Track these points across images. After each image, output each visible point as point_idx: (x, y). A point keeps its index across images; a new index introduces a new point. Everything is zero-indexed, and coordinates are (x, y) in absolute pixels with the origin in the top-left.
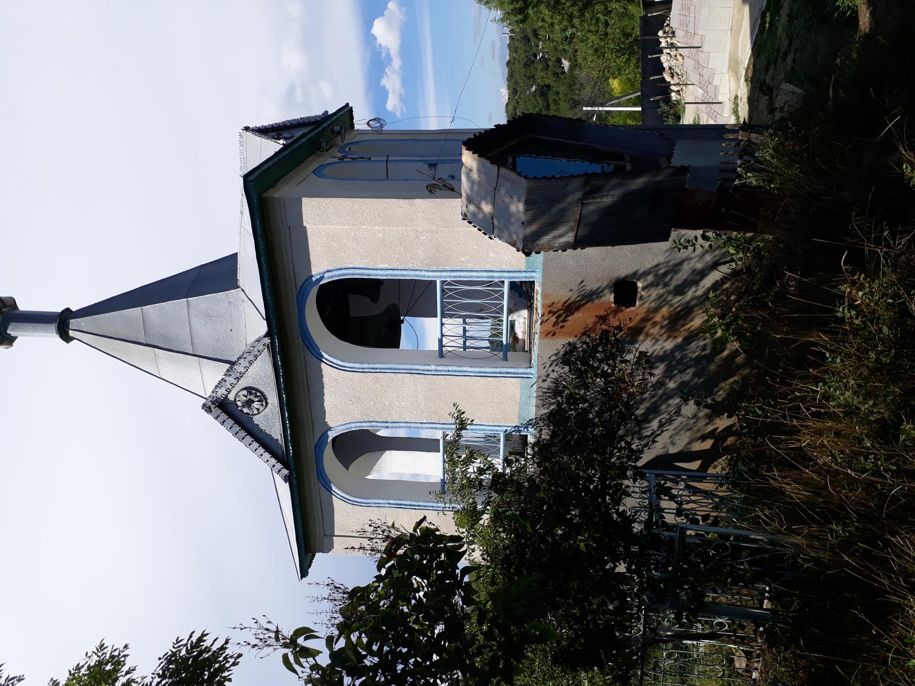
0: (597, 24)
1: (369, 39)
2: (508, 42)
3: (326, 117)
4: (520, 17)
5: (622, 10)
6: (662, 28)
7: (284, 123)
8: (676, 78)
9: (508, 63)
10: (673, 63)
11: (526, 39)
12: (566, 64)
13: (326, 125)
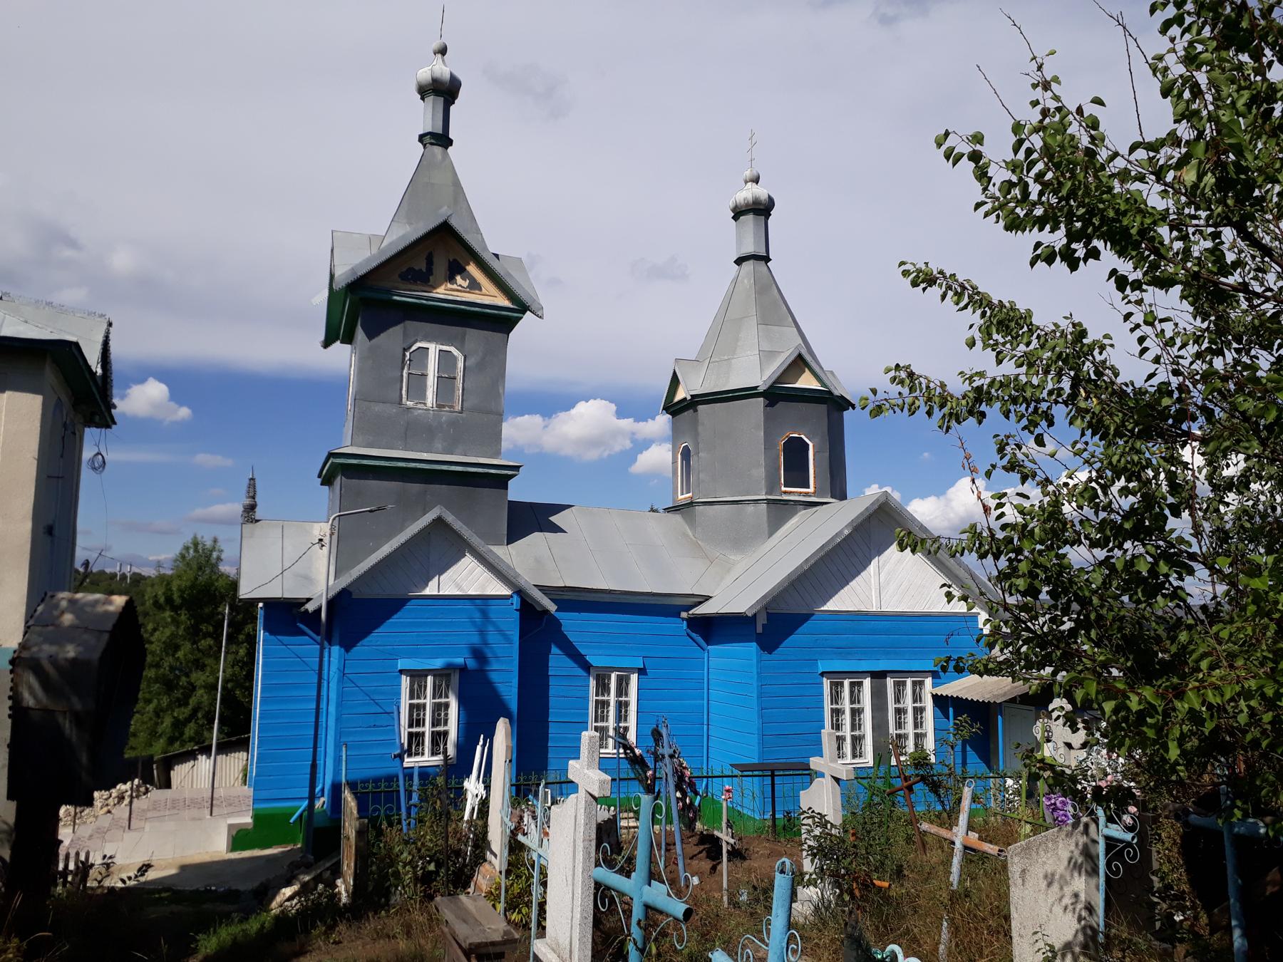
2: (108, 570)
5: (160, 731)
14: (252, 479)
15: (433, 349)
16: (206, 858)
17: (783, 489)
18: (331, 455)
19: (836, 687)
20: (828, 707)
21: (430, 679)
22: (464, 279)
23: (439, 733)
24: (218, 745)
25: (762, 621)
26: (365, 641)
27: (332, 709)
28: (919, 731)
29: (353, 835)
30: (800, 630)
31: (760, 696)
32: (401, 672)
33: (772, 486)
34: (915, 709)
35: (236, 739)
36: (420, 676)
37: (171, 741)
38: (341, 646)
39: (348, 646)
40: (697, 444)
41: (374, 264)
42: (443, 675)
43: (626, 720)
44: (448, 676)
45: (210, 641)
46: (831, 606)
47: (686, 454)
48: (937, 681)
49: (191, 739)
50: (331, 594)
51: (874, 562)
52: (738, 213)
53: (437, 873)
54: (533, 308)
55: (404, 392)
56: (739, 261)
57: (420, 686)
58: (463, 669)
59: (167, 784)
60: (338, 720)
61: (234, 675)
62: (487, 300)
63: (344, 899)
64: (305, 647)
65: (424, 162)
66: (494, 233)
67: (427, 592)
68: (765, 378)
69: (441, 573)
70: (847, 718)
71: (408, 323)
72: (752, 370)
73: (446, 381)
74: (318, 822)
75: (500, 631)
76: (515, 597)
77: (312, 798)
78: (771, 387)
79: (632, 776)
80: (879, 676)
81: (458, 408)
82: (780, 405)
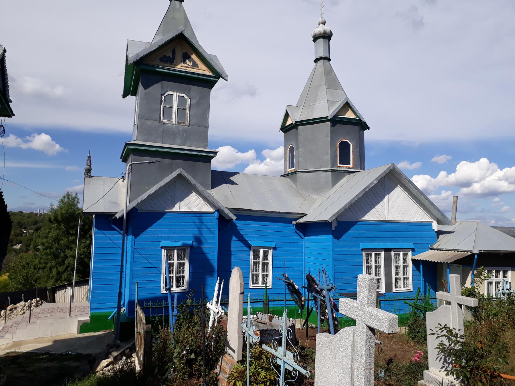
0: (45, 263)
1: (39, 131)
2: (34, 212)
3: (8, 101)
4: (53, 219)
5: (51, 276)
6: (41, 299)
7: (6, 74)
8: (9, 312)
9: (21, 212)
10: (19, 309)
11: (36, 223)
12: (18, 247)
13: (3, 100)
14: (89, 157)
15: (176, 95)
16: (68, 337)
17: (339, 165)
18: (127, 144)
19: (368, 256)
20: (364, 265)
21: (176, 251)
22: (190, 62)
23: (180, 277)
24: (76, 282)
25: (334, 225)
26: (145, 233)
27: (128, 265)
28: (405, 276)
29: (142, 333)
30: (352, 229)
31: (334, 260)
32: (162, 248)
33: (333, 164)
34: (404, 266)
35: (83, 281)
36: (172, 250)
37: (57, 280)
38: (133, 235)
39: (136, 235)
40: (297, 144)
41: (148, 52)
42: (182, 249)
43: (267, 271)
44: (184, 250)
45: (73, 237)
46: (366, 218)
47: (292, 150)
48: (414, 253)
49: (65, 280)
50: (128, 209)
51: (386, 197)
52: (316, 38)
53: (196, 359)
54: (223, 76)
55: (162, 115)
56: (316, 61)
57: (171, 255)
58: (191, 247)
59: (53, 300)
60: (131, 270)
61: (84, 252)
62: (201, 72)
63: (138, 368)
64: (115, 236)
65: (171, 8)
66: (205, 40)
67: (174, 209)
68: (331, 113)
69: (181, 201)
70: (401, 269)
71: (163, 82)
72: (325, 109)
73: (181, 110)
74: (122, 320)
75: (208, 229)
76: (216, 213)
77: (119, 308)
78: (334, 117)
79: (291, 298)
80: (388, 251)
81: (187, 124)
82: (338, 126)
